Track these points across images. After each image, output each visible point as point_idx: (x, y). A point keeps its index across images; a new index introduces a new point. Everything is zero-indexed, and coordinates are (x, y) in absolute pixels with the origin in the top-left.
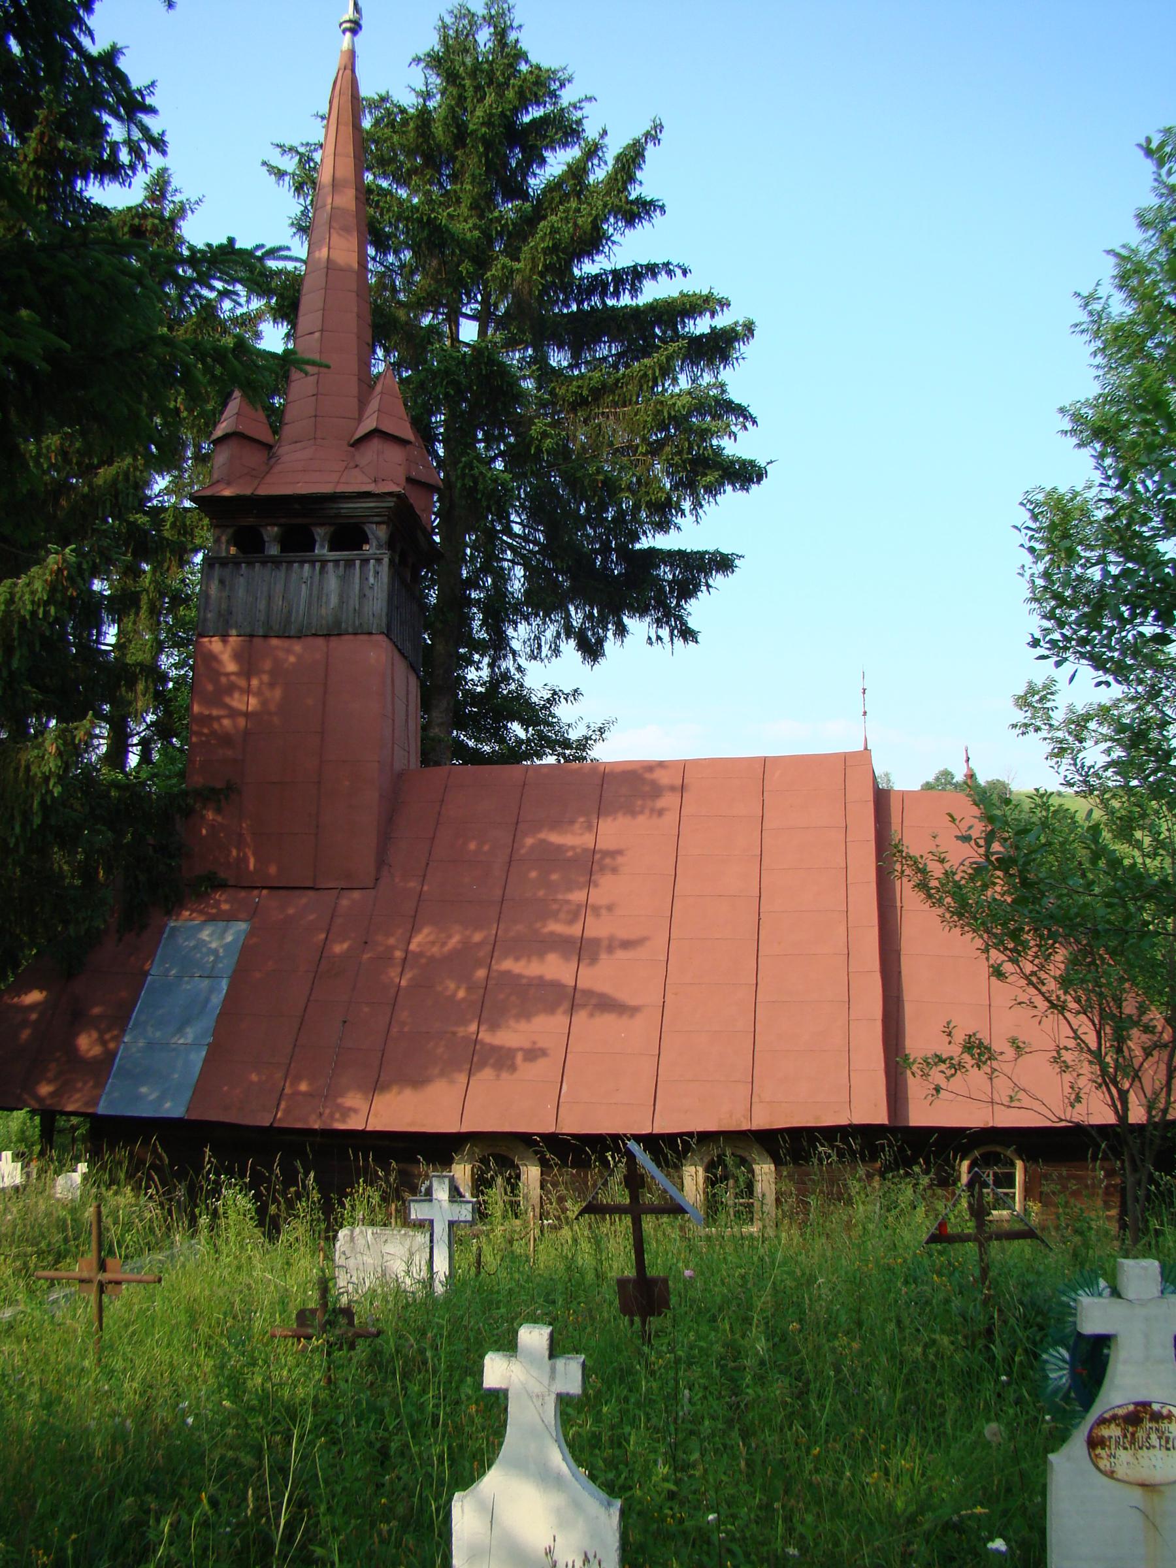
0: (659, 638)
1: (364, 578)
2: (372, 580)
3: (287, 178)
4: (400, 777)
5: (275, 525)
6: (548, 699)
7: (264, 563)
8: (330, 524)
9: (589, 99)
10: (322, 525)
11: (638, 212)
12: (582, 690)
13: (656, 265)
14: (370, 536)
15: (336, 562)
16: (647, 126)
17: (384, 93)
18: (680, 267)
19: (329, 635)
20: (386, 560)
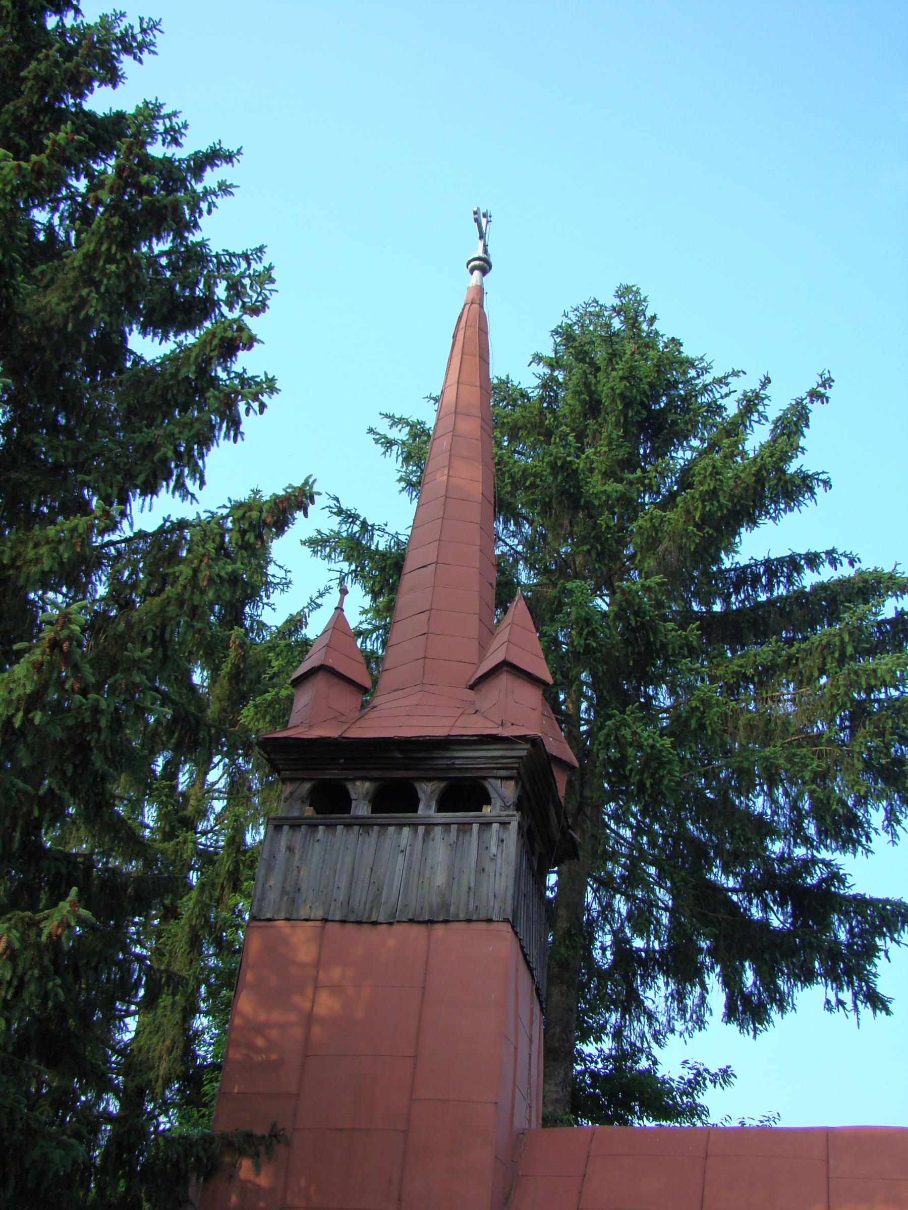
0: (840, 1003)
1: (483, 847)
2: (494, 849)
3: (395, 448)
4: (518, 1138)
5: (364, 779)
6: (689, 1081)
7: (348, 826)
8: (440, 779)
9: (735, 374)
10: (430, 779)
11: (795, 489)
12: (735, 1069)
13: (816, 555)
14: (493, 794)
15: (447, 825)
16: (813, 383)
17: (504, 378)
18: (846, 556)
19: (432, 922)
20: (514, 825)
